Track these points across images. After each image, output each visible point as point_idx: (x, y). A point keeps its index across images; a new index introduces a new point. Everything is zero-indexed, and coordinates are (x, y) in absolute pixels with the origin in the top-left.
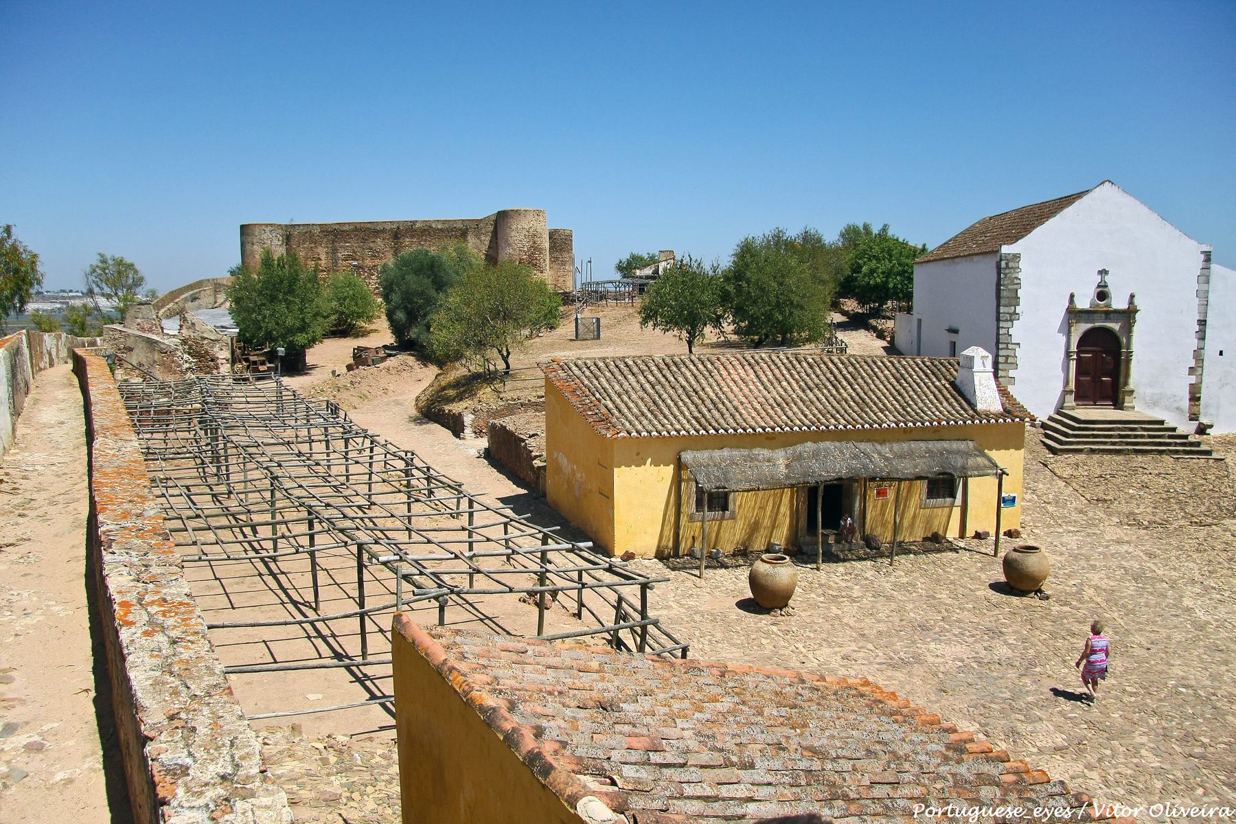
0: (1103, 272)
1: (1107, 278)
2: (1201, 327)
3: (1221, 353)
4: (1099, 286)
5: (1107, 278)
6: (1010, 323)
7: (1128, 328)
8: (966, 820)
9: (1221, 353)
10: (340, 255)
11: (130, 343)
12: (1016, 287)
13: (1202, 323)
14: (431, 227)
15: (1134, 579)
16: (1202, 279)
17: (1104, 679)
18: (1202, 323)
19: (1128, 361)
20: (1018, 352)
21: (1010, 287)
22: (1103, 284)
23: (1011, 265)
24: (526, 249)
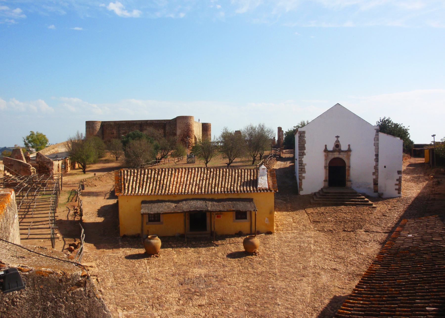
0: (338, 137)
1: (339, 138)
2: (377, 157)
3: (385, 167)
4: (336, 142)
5: (339, 139)
6: (302, 156)
7: (349, 157)
8: (1, 309)
9: (385, 167)
10: (121, 132)
11: (12, 163)
12: (304, 143)
13: (377, 155)
14: (153, 122)
15: (288, 246)
16: (376, 139)
17: (201, 275)
18: (377, 155)
19: (349, 170)
20: (306, 167)
21: (302, 143)
22: (337, 141)
23: (302, 135)
24: (186, 130)
